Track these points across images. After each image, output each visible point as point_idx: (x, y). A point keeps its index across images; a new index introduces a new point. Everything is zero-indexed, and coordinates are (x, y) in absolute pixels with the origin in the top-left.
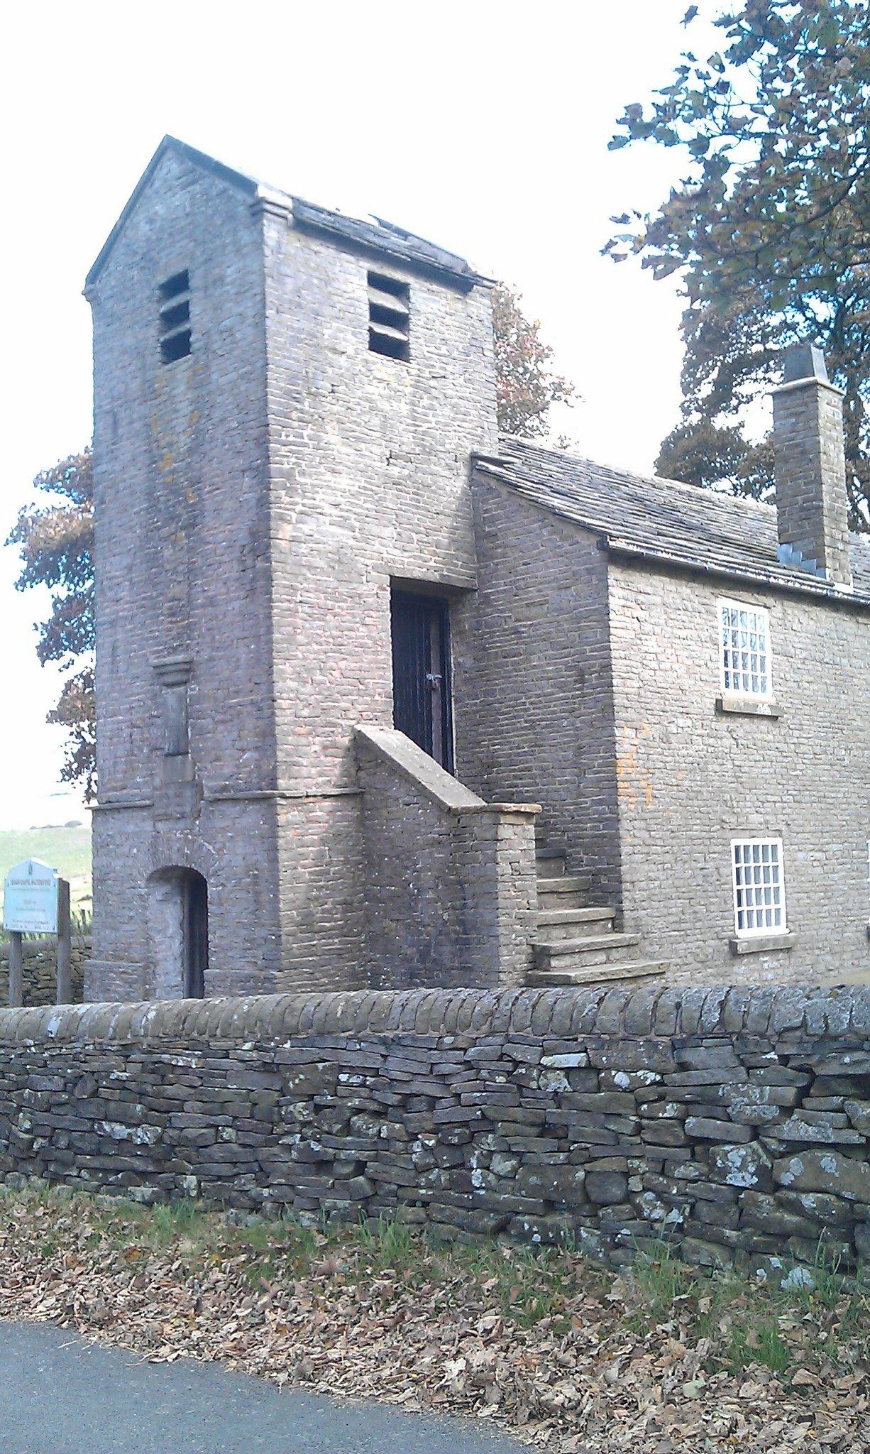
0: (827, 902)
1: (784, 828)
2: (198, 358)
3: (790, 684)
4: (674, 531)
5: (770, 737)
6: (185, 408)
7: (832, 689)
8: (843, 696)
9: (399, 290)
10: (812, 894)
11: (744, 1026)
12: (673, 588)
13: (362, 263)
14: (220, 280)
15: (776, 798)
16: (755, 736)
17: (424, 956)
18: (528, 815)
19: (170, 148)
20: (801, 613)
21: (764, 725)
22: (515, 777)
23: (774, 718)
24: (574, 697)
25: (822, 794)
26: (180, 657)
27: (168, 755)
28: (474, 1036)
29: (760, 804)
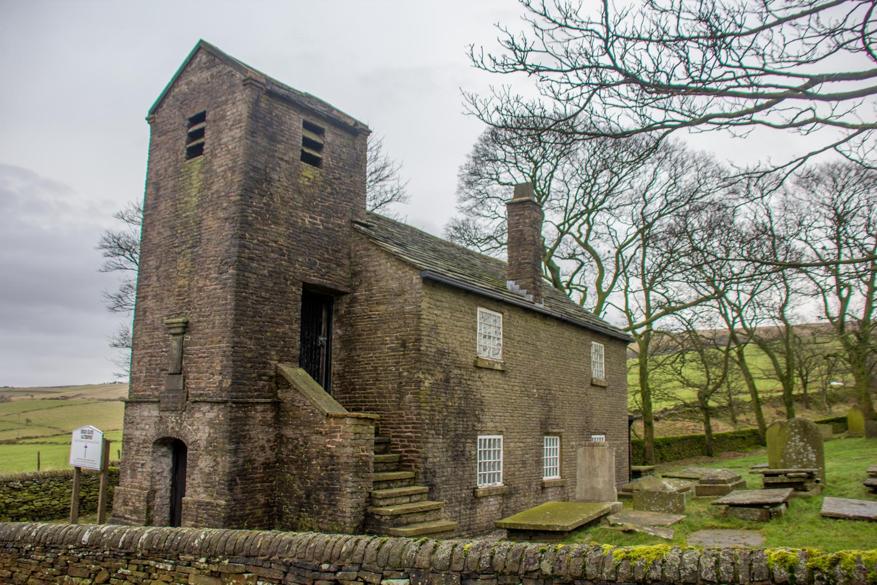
1: (504, 430)
2: (207, 158)
3: (511, 354)
4: (456, 269)
5: (501, 382)
6: (197, 184)
7: (531, 357)
9: (319, 131)
10: (516, 466)
11: (505, 567)
12: (455, 299)
13: (300, 116)
14: (223, 118)
15: (501, 414)
17: (308, 496)
18: (372, 420)
19: (202, 47)
21: (498, 376)
22: (364, 397)
23: (502, 372)
24: (399, 355)
26: (181, 320)
27: (170, 374)
28: (341, 564)
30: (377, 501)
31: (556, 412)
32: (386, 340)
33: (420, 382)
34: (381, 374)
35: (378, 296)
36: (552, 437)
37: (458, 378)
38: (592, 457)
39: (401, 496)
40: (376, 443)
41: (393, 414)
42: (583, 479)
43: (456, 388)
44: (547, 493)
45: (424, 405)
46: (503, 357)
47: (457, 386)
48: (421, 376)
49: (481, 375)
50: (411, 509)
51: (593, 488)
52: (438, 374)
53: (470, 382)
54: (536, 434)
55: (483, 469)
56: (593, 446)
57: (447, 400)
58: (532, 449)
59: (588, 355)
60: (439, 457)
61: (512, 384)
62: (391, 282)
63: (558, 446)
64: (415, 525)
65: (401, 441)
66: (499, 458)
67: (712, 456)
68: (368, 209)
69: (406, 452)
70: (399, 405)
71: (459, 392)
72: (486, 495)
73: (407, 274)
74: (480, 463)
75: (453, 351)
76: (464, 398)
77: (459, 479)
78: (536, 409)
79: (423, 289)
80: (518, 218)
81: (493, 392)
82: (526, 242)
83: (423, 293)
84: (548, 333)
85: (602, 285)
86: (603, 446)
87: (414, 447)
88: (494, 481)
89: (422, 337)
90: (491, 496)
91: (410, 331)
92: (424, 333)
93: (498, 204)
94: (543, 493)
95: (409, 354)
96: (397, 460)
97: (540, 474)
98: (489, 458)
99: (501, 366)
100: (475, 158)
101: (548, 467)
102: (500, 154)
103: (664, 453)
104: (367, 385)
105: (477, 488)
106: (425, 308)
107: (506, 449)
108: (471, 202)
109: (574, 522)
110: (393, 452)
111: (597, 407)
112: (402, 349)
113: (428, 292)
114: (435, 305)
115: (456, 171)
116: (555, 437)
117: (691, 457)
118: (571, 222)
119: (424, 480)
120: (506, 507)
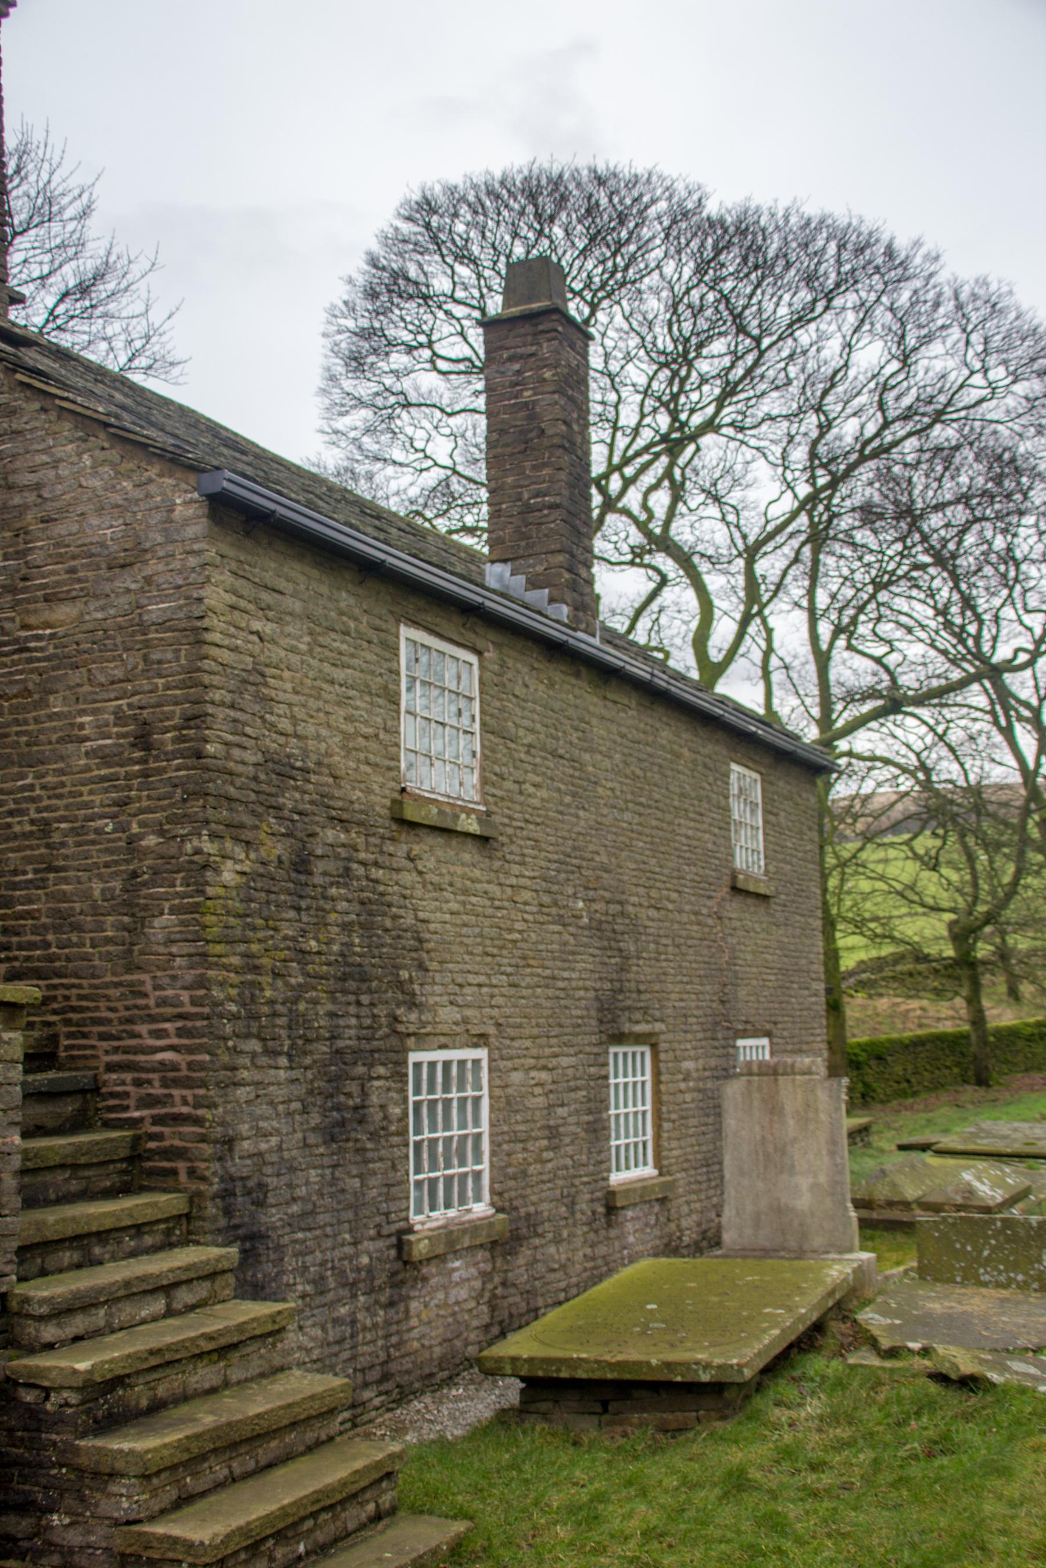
0: (551, 1154)
1: (492, 1030)
3: (508, 785)
5: (477, 873)
7: (568, 799)
8: (581, 813)
10: (530, 1145)
12: (324, 589)
15: (482, 979)
16: (452, 869)
20: (525, 670)
21: (469, 854)
23: (483, 840)
24: (128, 777)
25: (548, 972)
29: (457, 989)
30: (31, 1328)
31: (642, 971)
32: (81, 727)
33: (205, 867)
34: (63, 844)
35: (54, 574)
36: (629, 1049)
37: (337, 857)
38: (774, 1109)
39: (128, 1296)
40: (32, 1095)
41: (106, 986)
42: (746, 1182)
43: (333, 891)
44: (621, 1225)
45: (219, 949)
46: (484, 794)
47: (338, 885)
48: (209, 847)
49: (416, 849)
50: (169, 1348)
51: (779, 1210)
52: (269, 842)
53: (378, 874)
54: (587, 1039)
55: (426, 1165)
56: (775, 1073)
57: (304, 932)
58: (577, 1089)
59: (723, 803)
60: (278, 1132)
61: (513, 881)
62: (95, 521)
63: (648, 1077)
64: (184, 1409)
65: (138, 1083)
66: (477, 1122)
67: (988, 1086)
68: (12, 282)
69: (157, 1120)
70: (130, 951)
71: (343, 905)
72: (440, 1250)
73: (152, 488)
74: (418, 1145)
75: (319, 764)
76: (362, 925)
77: (350, 1206)
78: (585, 963)
79: (209, 537)
80: (517, 367)
81: (454, 906)
82: (546, 442)
83: (211, 554)
84: (614, 728)
85: (710, 643)
86: (809, 1072)
87: (185, 1102)
88: (463, 1201)
89: (210, 709)
90: (456, 1254)
91: (167, 688)
92: (217, 695)
93: (434, 433)
94: (609, 1225)
95: (164, 770)
96: (124, 1153)
97: (601, 1166)
98: (447, 1126)
99: (480, 821)
100: (372, 294)
101: (622, 1142)
102: (441, 284)
103: (869, 1079)
104: (14, 886)
105: (410, 1230)
106: (220, 607)
107: (498, 1092)
108: (361, 416)
109: (758, 1346)
110: (108, 1125)
111: (749, 957)
112: (138, 754)
113: (231, 552)
114: (256, 601)
115: (318, 321)
116: (639, 1049)
117: (936, 1088)
118: (629, 471)
119: (222, 1222)
120: (504, 1284)
